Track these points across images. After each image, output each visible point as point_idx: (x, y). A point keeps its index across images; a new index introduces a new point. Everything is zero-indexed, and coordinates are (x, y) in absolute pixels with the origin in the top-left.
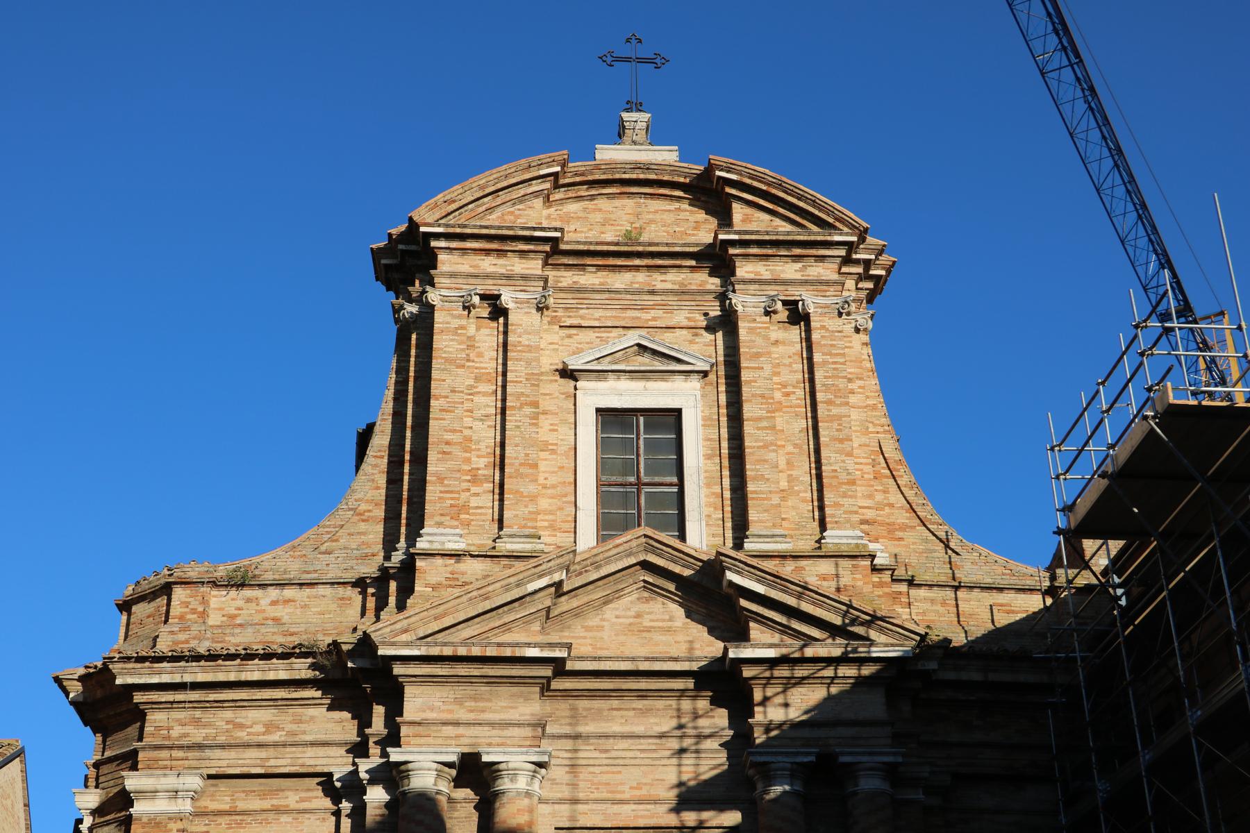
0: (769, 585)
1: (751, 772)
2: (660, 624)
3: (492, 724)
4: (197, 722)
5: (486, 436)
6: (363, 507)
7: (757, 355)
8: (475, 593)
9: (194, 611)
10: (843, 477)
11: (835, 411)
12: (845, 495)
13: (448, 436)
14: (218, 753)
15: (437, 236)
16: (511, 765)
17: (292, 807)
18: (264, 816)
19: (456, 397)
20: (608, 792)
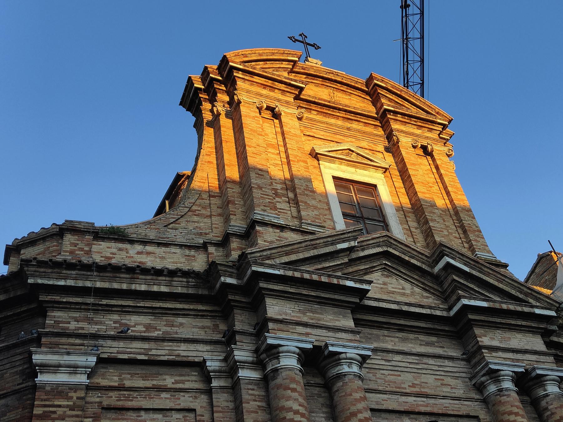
0: (471, 268)
2: (399, 291)
3: (328, 328)
4: (90, 321)
6: (194, 208)
8: (309, 243)
9: (82, 249)
14: (109, 343)
15: (239, 69)
16: (349, 355)
17: (169, 386)
18: (147, 393)
20: (396, 387)
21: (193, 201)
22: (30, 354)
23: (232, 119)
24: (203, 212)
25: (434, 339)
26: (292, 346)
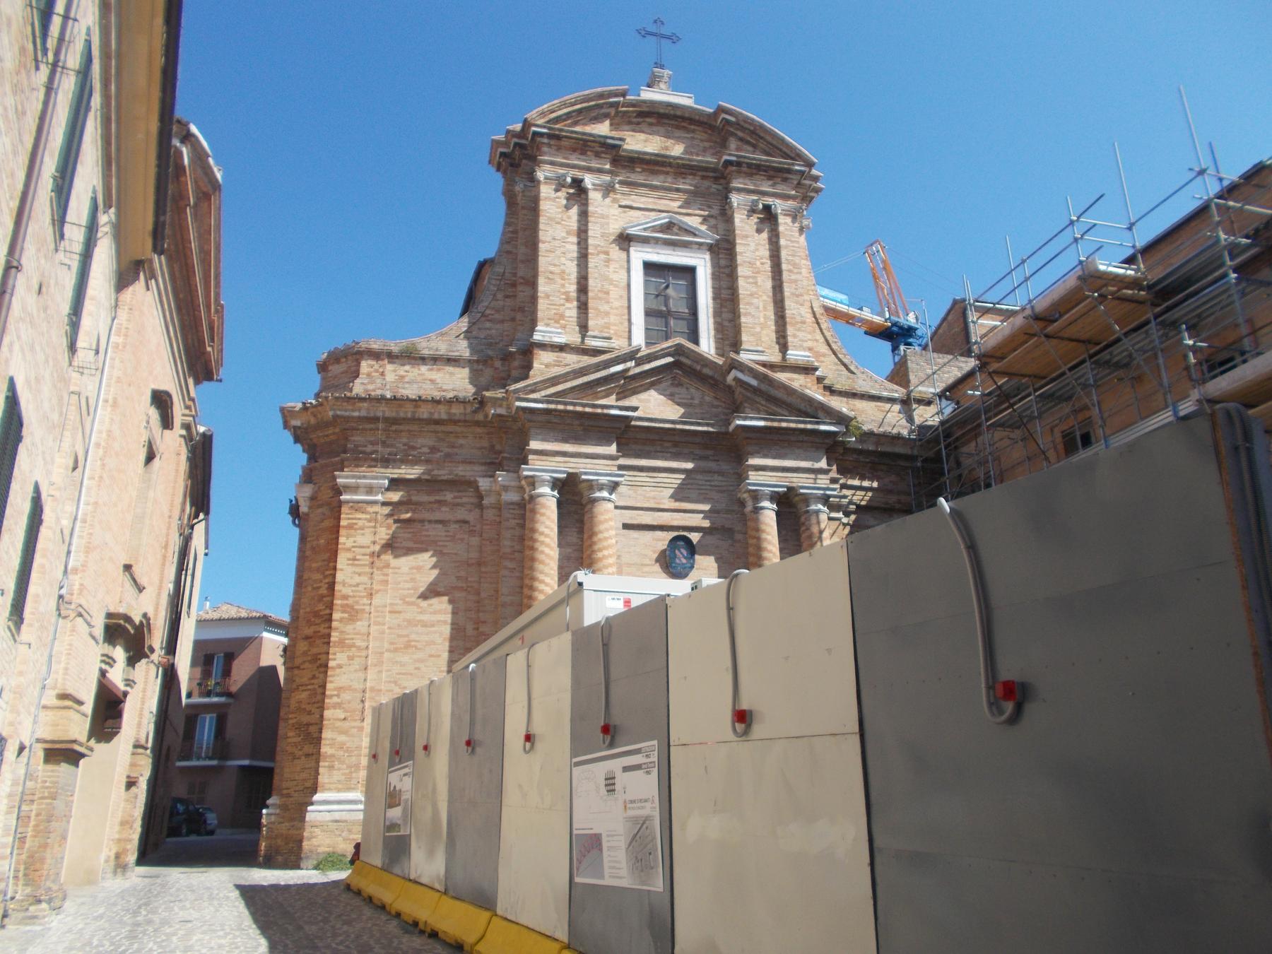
1: (745, 495)
5: (572, 269)
6: (488, 312)
7: (747, 236)
9: (377, 371)
10: (798, 319)
11: (793, 277)
12: (799, 330)
13: (552, 268)
19: (557, 243)
21: (486, 304)
22: (334, 478)
23: (312, 458)
24: (497, 316)
25: (710, 452)
26: (547, 476)
